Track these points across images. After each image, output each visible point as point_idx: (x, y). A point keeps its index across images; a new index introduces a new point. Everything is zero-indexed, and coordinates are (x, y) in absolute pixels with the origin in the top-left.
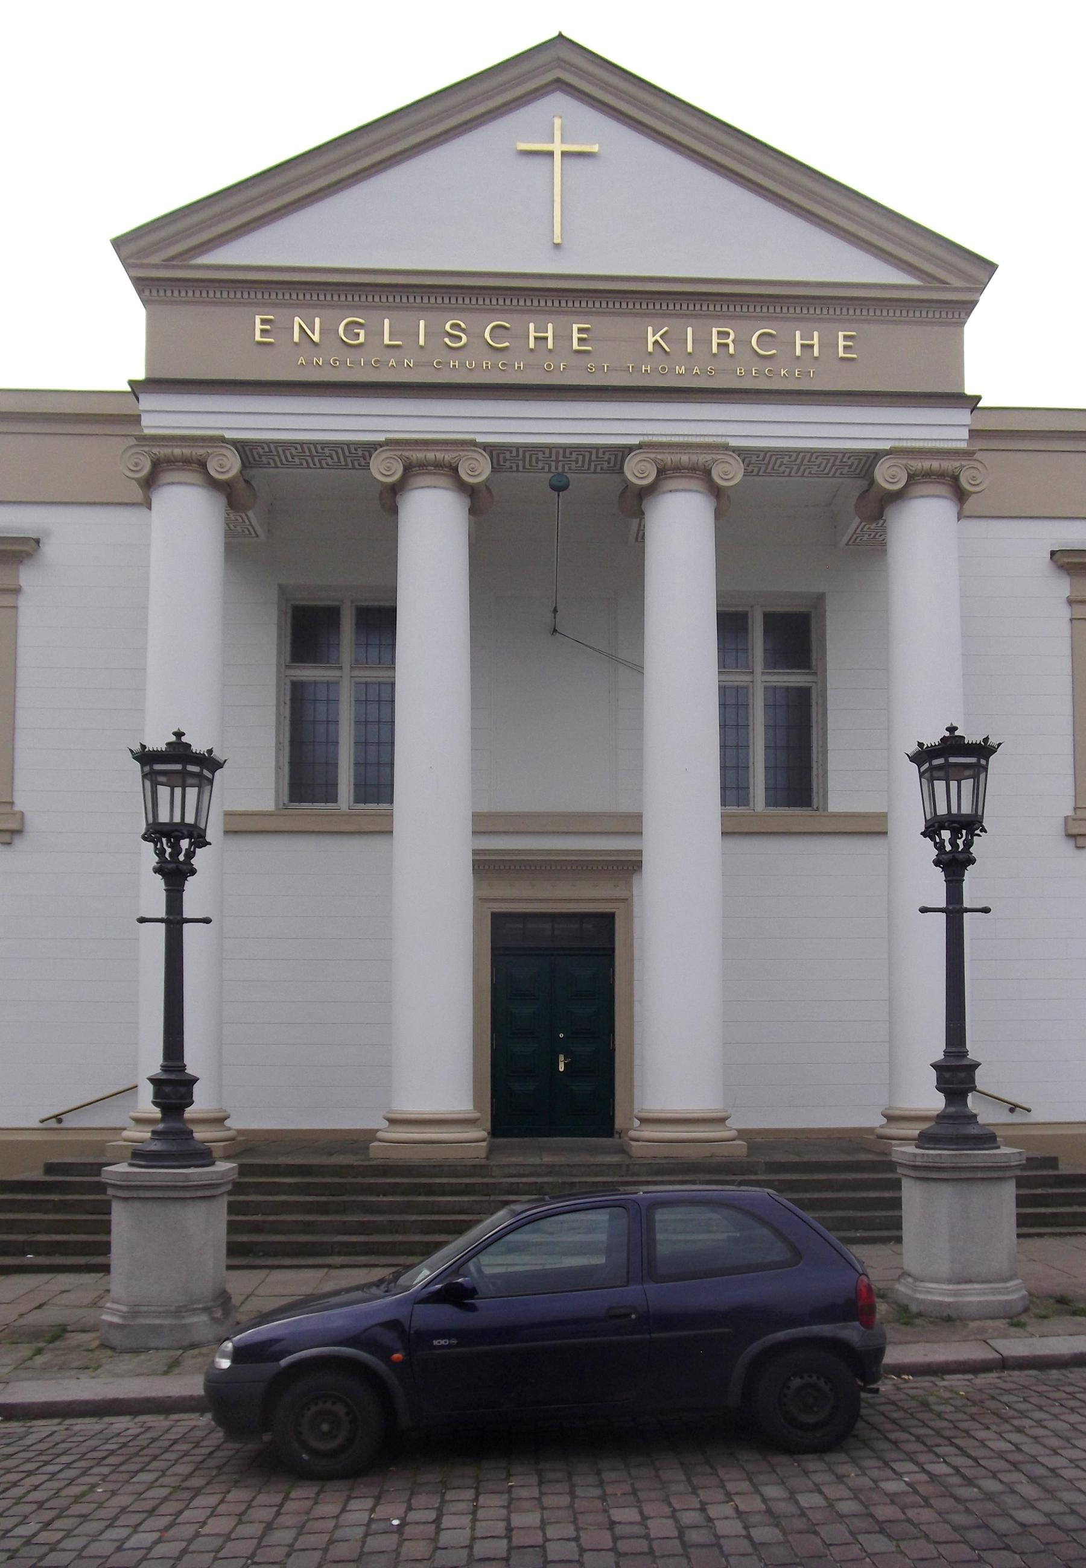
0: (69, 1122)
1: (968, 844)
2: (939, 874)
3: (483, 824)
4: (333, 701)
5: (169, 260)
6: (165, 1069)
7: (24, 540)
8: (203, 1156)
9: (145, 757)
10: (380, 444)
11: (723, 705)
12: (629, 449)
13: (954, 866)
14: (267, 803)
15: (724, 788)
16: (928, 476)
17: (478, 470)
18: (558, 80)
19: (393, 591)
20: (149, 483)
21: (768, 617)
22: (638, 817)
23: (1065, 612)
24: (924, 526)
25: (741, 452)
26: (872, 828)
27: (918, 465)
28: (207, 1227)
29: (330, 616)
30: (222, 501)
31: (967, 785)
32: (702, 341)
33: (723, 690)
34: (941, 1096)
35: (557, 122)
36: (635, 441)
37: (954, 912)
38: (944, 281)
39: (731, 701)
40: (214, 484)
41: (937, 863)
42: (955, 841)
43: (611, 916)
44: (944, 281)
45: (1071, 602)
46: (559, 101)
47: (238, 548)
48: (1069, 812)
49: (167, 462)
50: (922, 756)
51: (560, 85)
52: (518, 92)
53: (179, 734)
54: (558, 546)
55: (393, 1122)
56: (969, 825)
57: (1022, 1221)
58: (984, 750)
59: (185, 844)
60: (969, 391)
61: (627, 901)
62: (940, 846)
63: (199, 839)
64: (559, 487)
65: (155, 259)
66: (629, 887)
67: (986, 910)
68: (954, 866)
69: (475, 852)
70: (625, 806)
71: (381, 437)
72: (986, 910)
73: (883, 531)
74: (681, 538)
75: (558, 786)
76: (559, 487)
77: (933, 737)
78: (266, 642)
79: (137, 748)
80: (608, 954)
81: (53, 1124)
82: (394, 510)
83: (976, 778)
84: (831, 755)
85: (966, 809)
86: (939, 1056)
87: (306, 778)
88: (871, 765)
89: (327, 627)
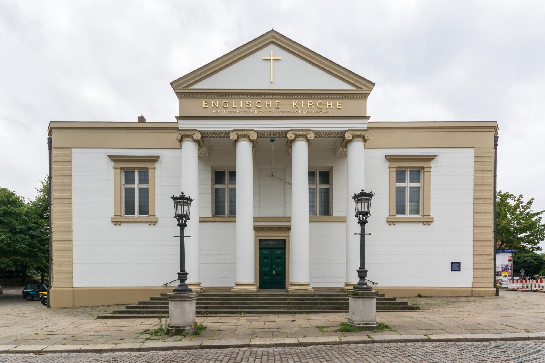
0: (169, 285)
1: (366, 218)
2: (359, 225)
3: (256, 219)
4: (224, 192)
5: (185, 88)
6: (360, 268)
7: (156, 156)
8: (190, 291)
9: (174, 198)
10: (232, 131)
11: (310, 193)
12: (289, 131)
13: (363, 223)
14: (210, 215)
15: (310, 211)
16: (357, 136)
17: (254, 136)
18: (272, 41)
19: (235, 167)
20: (181, 141)
21: (320, 172)
22: (290, 218)
23: (388, 170)
24: (356, 148)
25: (314, 131)
26: (343, 220)
27: (355, 133)
28: (190, 307)
29: (223, 173)
30: (197, 145)
31: (366, 204)
32: (305, 105)
33: (310, 189)
34: (359, 278)
35: (272, 52)
36: (290, 129)
37: (362, 235)
38: (361, 88)
39: (311, 191)
40: (195, 141)
41: (358, 223)
42: (363, 217)
43: (284, 240)
44: (360, 88)
45: (389, 168)
46: (272, 46)
47: (201, 158)
48: (388, 216)
49: (184, 136)
50: (356, 197)
51: (272, 42)
52: (263, 44)
53: (182, 193)
54: (273, 154)
55: (237, 285)
56: (366, 214)
57: (377, 308)
58: (371, 195)
59: (184, 219)
60: (367, 115)
61: (288, 236)
62: (359, 219)
63: (188, 218)
64: (272, 141)
65: (181, 87)
66: (289, 233)
67: (370, 234)
68: (363, 223)
69: (254, 226)
70: (288, 215)
71: (232, 129)
72: (370, 234)
73: (346, 151)
74: (300, 152)
75: (273, 211)
76: (272, 141)
77: (358, 192)
78: (209, 178)
79: (172, 196)
80: (284, 248)
81: (165, 286)
82: (235, 147)
83: (368, 202)
84: (334, 203)
85: (366, 209)
86: (179, 271)
87: (218, 210)
88: (344, 205)
89: (222, 177)
